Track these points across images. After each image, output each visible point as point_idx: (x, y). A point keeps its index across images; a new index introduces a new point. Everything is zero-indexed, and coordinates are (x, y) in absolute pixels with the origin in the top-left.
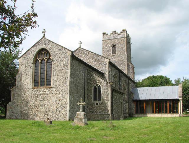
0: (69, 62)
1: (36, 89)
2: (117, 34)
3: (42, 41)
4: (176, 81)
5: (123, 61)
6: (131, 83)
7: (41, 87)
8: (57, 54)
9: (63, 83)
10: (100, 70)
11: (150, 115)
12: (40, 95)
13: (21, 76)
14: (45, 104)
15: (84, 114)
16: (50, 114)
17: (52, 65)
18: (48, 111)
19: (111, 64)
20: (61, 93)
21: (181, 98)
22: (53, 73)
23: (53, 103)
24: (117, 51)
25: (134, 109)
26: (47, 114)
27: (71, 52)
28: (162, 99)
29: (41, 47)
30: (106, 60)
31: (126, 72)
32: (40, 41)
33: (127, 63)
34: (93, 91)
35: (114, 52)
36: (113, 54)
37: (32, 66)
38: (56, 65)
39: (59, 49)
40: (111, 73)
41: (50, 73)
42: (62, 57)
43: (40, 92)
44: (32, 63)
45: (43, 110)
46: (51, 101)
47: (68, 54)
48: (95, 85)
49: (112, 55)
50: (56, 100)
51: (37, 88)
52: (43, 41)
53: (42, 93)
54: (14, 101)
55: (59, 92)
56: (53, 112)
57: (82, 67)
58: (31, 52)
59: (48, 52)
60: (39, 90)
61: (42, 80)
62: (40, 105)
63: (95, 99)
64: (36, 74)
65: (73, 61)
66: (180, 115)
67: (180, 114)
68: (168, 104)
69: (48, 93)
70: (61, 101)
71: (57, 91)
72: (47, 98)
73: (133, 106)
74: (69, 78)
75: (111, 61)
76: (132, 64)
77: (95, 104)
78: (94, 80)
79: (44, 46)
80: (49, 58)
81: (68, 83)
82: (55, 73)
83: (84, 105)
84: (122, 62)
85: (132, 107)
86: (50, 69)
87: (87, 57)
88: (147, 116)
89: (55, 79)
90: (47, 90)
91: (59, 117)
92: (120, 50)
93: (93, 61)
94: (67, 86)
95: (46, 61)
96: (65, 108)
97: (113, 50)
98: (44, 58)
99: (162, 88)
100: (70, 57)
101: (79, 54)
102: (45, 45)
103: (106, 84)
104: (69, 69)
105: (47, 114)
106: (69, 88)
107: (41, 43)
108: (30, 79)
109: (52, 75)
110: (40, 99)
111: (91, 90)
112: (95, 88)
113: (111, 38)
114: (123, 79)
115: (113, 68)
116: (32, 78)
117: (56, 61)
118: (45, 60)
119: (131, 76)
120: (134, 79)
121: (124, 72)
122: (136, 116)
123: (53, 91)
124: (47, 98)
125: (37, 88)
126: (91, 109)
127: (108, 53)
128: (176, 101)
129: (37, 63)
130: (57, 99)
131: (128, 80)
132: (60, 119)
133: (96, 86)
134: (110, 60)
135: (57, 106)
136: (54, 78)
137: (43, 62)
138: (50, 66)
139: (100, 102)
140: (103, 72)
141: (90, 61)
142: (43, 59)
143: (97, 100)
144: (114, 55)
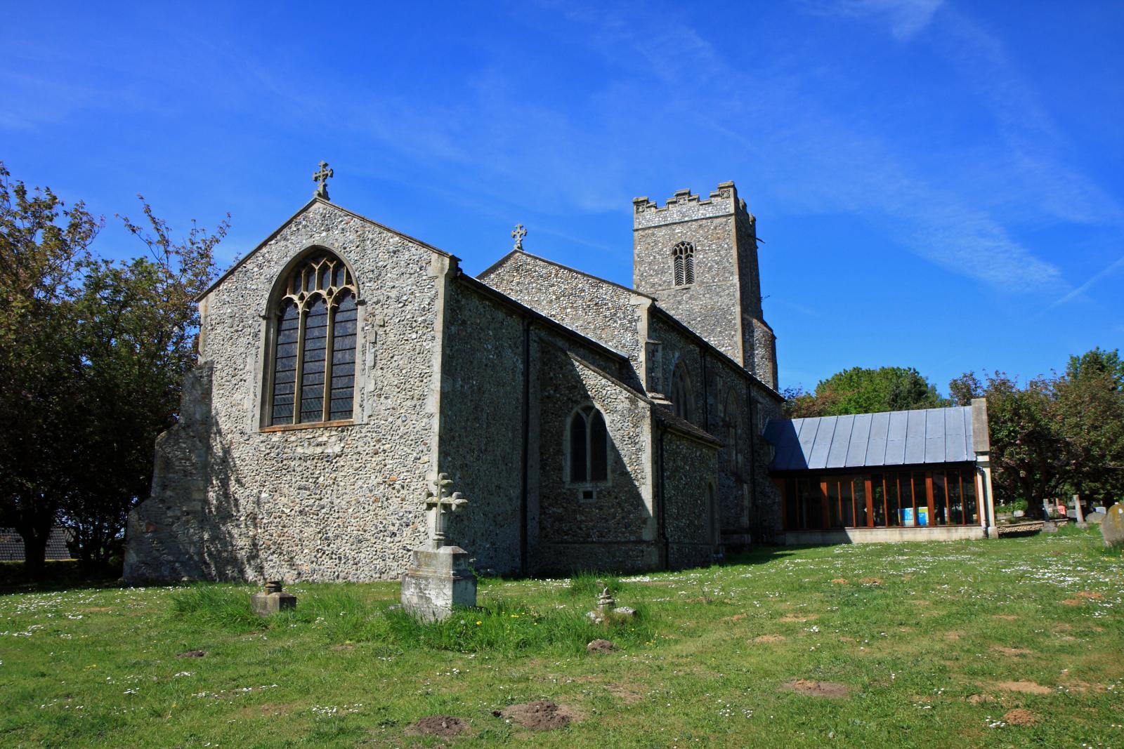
0: (439, 305)
1: (279, 434)
2: (694, 203)
3: (311, 215)
4: (954, 385)
5: (727, 311)
6: (761, 400)
7: (304, 424)
8: (383, 273)
9: (409, 403)
10: (610, 346)
11: (858, 536)
12: (297, 463)
13: (210, 376)
14: (322, 503)
15: (456, 557)
16: (346, 549)
17: (360, 324)
18: (337, 537)
19: (656, 314)
20: (402, 450)
21: (986, 458)
22: (363, 358)
23: (362, 499)
24: (695, 270)
25: (776, 508)
26: (328, 550)
27: (447, 261)
28: (441, 407)
29: (306, 243)
30: (634, 300)
31: (741, 355)
32: (301, 217)
33: (743, 319)
34: (567, 434)
35: (685, 274)
36: (678, 283)
37: (263, 328)
38: (378, 320)
39: (392, 249)
40: (659, 355)
41: (348, 358)
42: (407, 284)
43: (300, 450)
44: (264, 318)
45: (309, 531)
46: (355, 496)
47: (431, 271)
48: (577, 409)
49: (678, 287)
50: (373, 481)
51: (284, 431)
52: (318, 217)
53: (309, 451)
54: (169, 493)
55: (387, 446)
56: (360, 541)
57: (514, 323)
58: (260, 267)
59: (340, 264)
60: (293, 438)
61: (308, 390)
62: (297, 508)
63: (578, 475)
64: (285, 366)
65: (458, 301)
66: (986, 533)
67: (988, 525)
68: (929, 482)
69: (337, 449)
70: (397, 487)
71: (379, 441)
72: (333, 475)
73: (775, 497)
74: (437, 377)
75: (662, 305)
76: (765, 324)
77: (581, 496)
78: (578, 386)
79: (319, 239)
80: (346, 292)
81: (433, 404)
82: (370, 358)
83: (454, 508)
84: (716, 317)
85: (769, 501)
86: (348, 341)
87: (551, 289)
88: (848, 541)
89: (371, 387)
90: (333, 439)
91: (389, 562)
92: (711, 268)
93: (576, 309)
94: (431, 416)
95: (329, 306)
96: (417, 520)
97: (678, 267)
98: (320, 291)
99: (899, 416)
100: (440, 284)
101: (516, 280)
102: (324, 234)
103: (627, 404)
104: (439, 336)
105: (328, 550)
106: (435, 424)
107: (305, 227)
108: (252, 390)
109: (358, 367)
110: (297, 480)
111: (560, 433)
112: (578, 425)
113: (669, 220)
114: (720, 382)
115: (674, 337)
116: (260, 384)
117: (377, 303)
118: (325, 301)
119: (762, 374)
120: (776, 386)
121: (729, 355)
122: (790, 538)
123: (360, 441)
124: (333, 475)
125: (284, 431)
126: (560, 519)
127: (661, 279)
128: (967, 470)
129: (289, 312)
130: (380, 479)
131: (748, 388)
132: (394, 573)
133: (584, 415)
134: (654, 300)
135: (381, 513)
136: (364, 383)
137: (318, 307)
138: (349, 325)
139: (602, 485)
140: (623, 353)
141: (565, 308)
142: (317, 297)
143: (588, 478)
144: (683, 286)
